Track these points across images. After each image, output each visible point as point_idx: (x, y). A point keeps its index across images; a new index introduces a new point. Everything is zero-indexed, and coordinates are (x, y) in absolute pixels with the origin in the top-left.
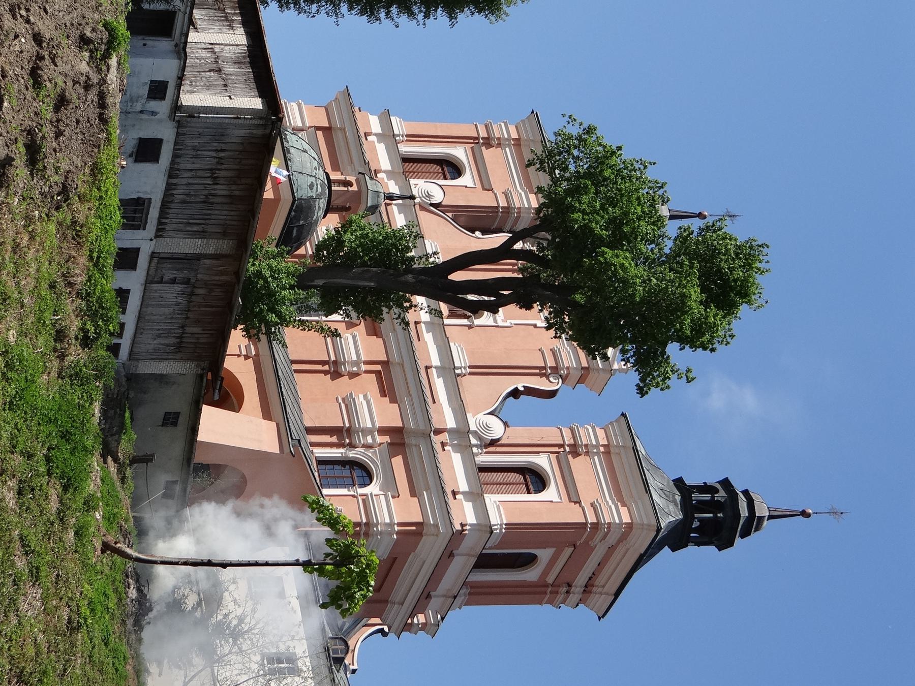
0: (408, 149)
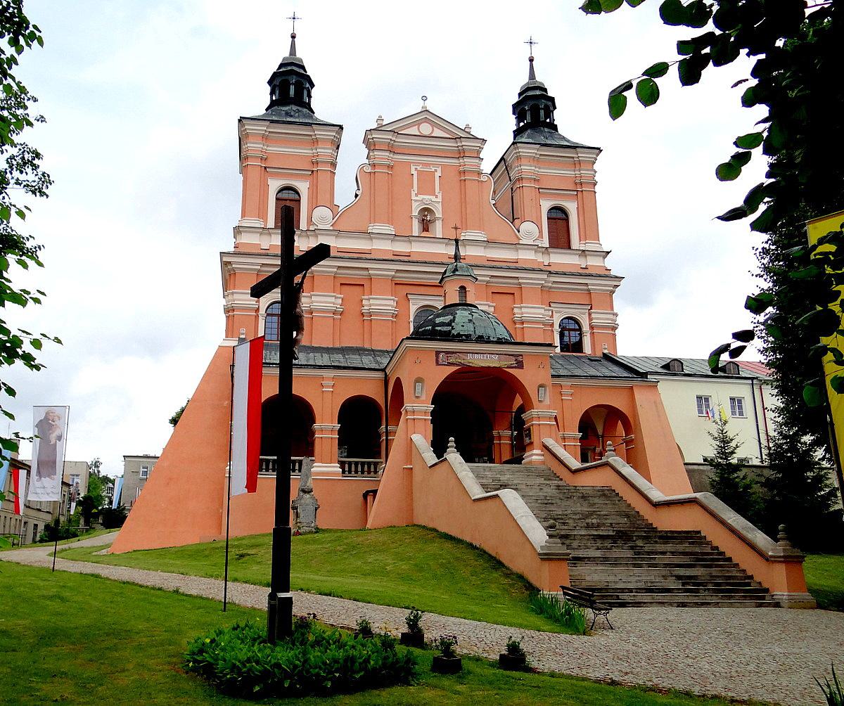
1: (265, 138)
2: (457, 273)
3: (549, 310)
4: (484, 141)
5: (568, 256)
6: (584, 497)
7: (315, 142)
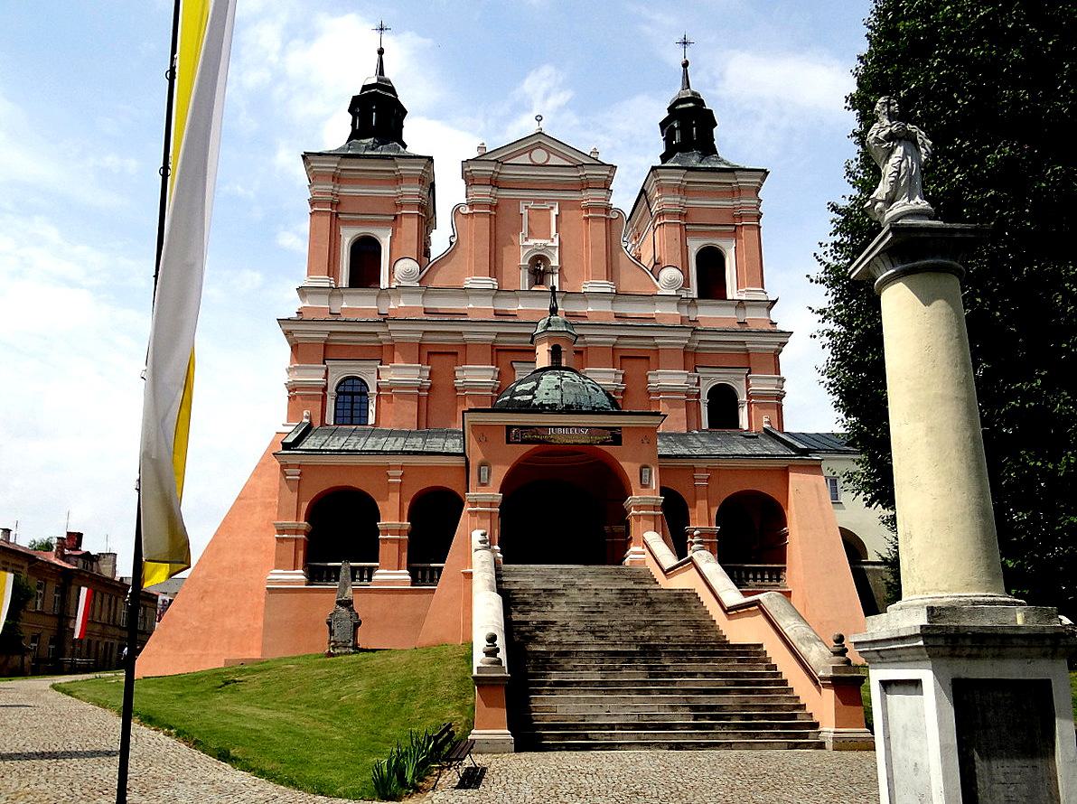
0: (344, 280)
2: (549, 329)
3: (694, 377)
4: (614, 168)
5: (711, 308)
6: (650, 604)
7: (398, 180)
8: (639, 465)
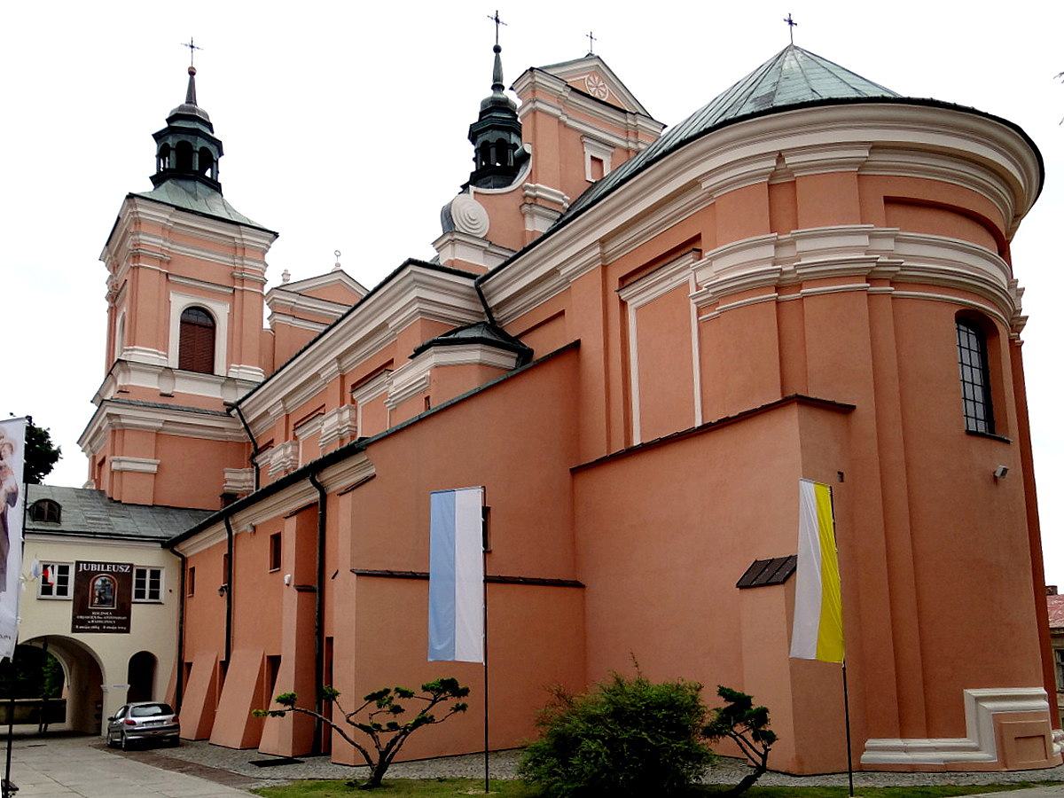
1: (167, 231)
8: (857, 395)
